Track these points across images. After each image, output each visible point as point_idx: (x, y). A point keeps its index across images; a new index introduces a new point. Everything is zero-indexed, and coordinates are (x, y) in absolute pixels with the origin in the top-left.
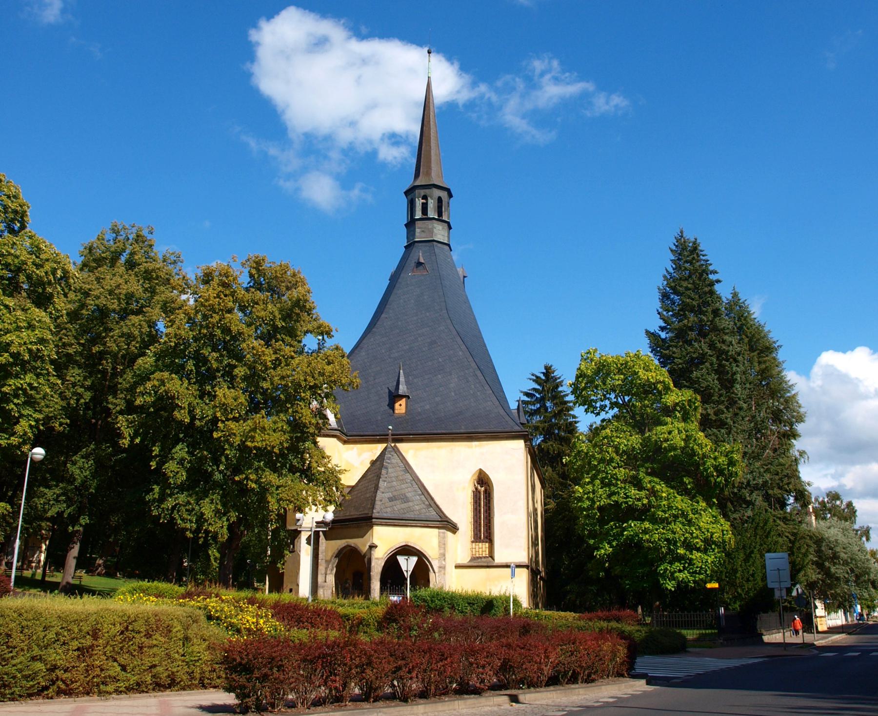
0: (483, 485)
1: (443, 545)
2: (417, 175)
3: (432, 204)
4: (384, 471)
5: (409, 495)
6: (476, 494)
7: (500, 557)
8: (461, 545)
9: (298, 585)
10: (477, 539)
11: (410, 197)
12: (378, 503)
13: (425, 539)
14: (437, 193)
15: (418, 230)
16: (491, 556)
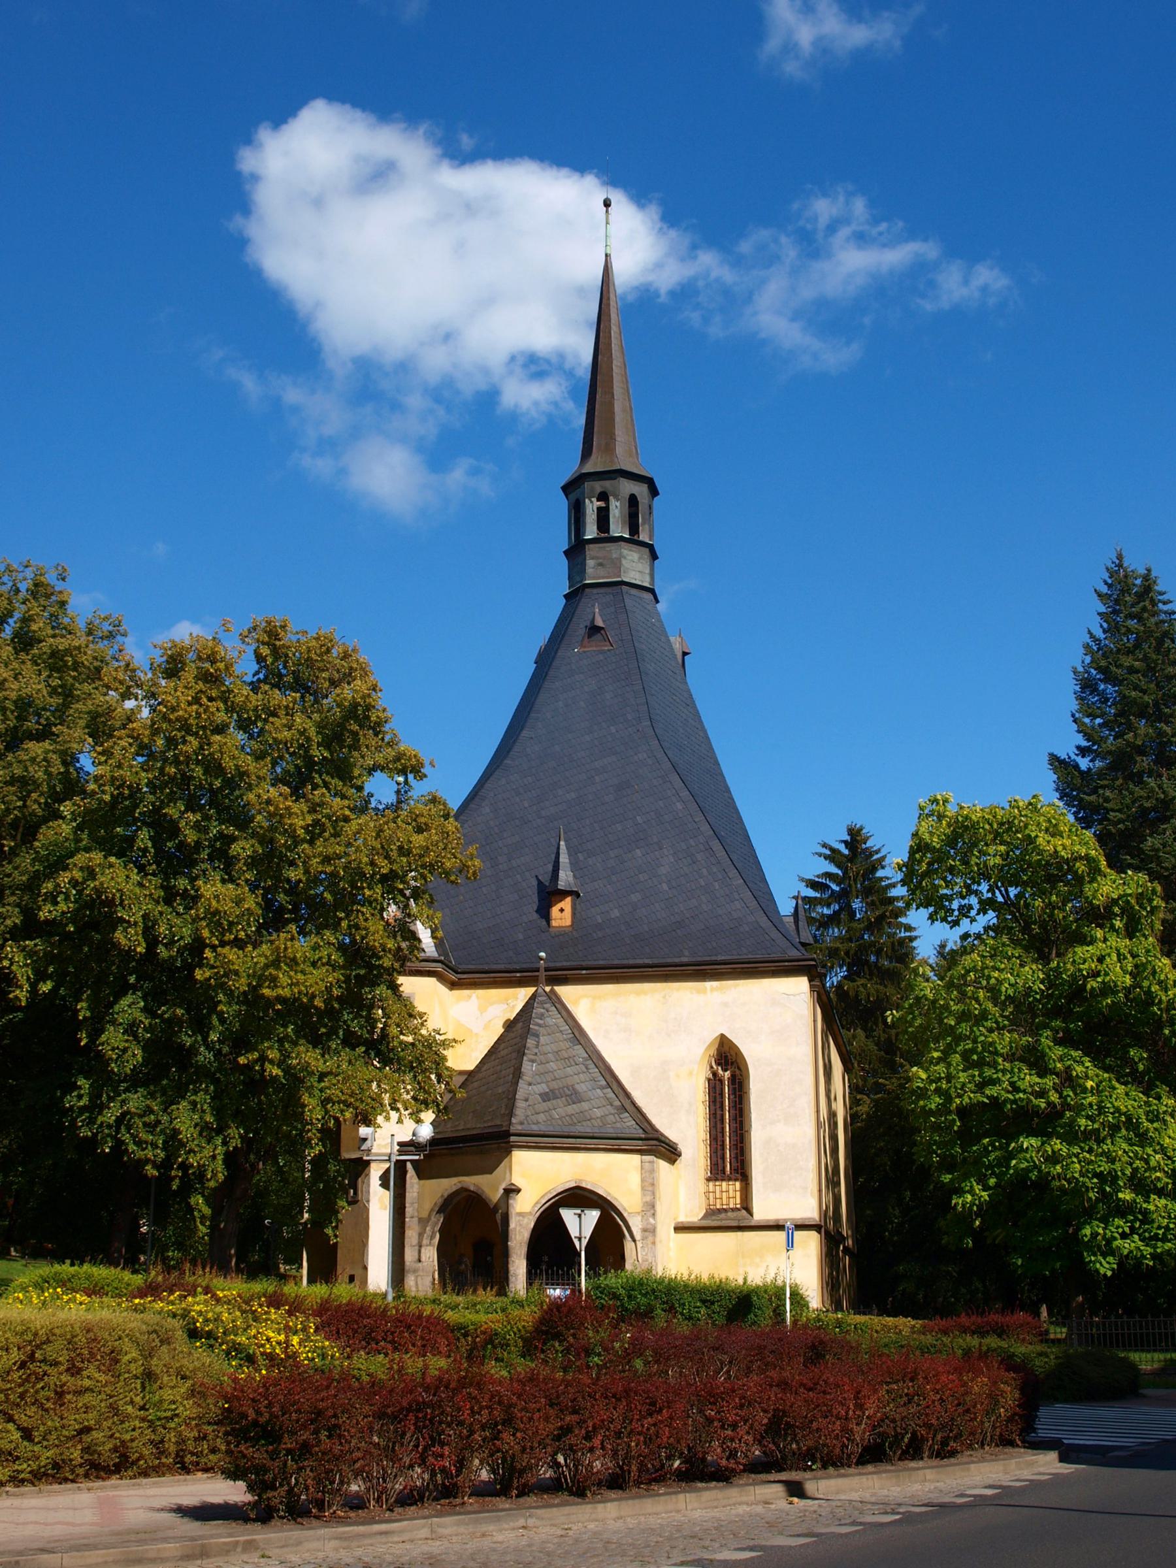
0: (729, 1076)
1: (649, 1185)
2: (587, 453)
3: (617, 509)
4: (530, 1042)
6: (714, 1084)
7: (762, 1211)
9: (365, 1268)
10: (717, 1173)
13: (616, 1175)
14: (628, 487)
15: (590, 563)
16: (747, 1206)
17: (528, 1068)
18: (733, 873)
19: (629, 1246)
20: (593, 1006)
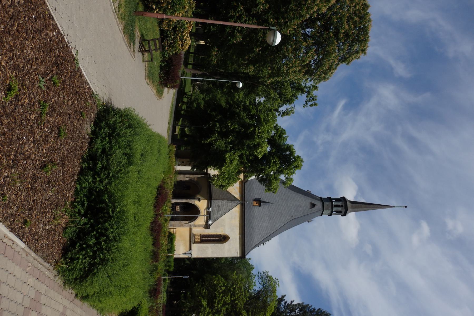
0: (223, 239)
1: (199, 226)
2: (351, 202)
3: (339, 209)
4: (230, 201)
5: (220, 212)
6: (220, 236)
7: (194, 246)
8: (199, 231)
9: (185, 166)
10: (202, 236)
11: (342, 199)
12: (217, 201)
13: (201, 220)
14: (343, 211)
15: (328, 203)
16: (195, 242)
17: (224, 202)
18: (263, 239)
19: (187, 222)
20: (236, 210)
